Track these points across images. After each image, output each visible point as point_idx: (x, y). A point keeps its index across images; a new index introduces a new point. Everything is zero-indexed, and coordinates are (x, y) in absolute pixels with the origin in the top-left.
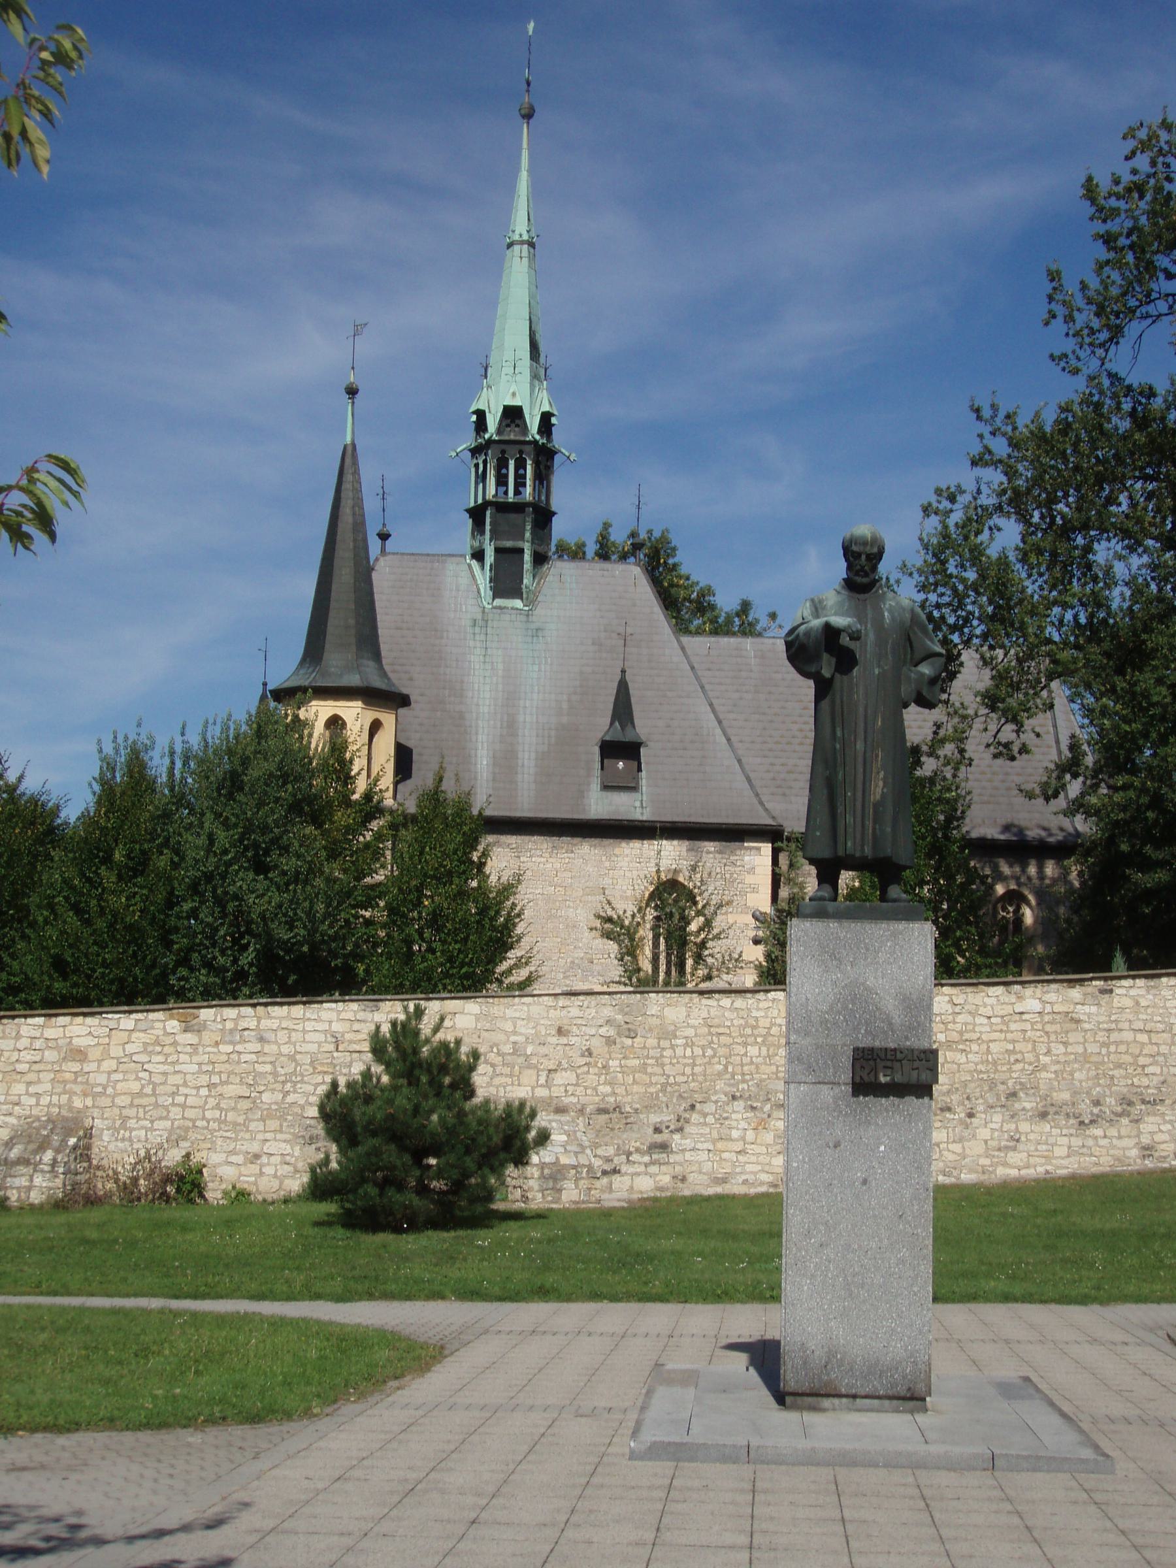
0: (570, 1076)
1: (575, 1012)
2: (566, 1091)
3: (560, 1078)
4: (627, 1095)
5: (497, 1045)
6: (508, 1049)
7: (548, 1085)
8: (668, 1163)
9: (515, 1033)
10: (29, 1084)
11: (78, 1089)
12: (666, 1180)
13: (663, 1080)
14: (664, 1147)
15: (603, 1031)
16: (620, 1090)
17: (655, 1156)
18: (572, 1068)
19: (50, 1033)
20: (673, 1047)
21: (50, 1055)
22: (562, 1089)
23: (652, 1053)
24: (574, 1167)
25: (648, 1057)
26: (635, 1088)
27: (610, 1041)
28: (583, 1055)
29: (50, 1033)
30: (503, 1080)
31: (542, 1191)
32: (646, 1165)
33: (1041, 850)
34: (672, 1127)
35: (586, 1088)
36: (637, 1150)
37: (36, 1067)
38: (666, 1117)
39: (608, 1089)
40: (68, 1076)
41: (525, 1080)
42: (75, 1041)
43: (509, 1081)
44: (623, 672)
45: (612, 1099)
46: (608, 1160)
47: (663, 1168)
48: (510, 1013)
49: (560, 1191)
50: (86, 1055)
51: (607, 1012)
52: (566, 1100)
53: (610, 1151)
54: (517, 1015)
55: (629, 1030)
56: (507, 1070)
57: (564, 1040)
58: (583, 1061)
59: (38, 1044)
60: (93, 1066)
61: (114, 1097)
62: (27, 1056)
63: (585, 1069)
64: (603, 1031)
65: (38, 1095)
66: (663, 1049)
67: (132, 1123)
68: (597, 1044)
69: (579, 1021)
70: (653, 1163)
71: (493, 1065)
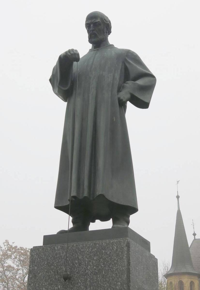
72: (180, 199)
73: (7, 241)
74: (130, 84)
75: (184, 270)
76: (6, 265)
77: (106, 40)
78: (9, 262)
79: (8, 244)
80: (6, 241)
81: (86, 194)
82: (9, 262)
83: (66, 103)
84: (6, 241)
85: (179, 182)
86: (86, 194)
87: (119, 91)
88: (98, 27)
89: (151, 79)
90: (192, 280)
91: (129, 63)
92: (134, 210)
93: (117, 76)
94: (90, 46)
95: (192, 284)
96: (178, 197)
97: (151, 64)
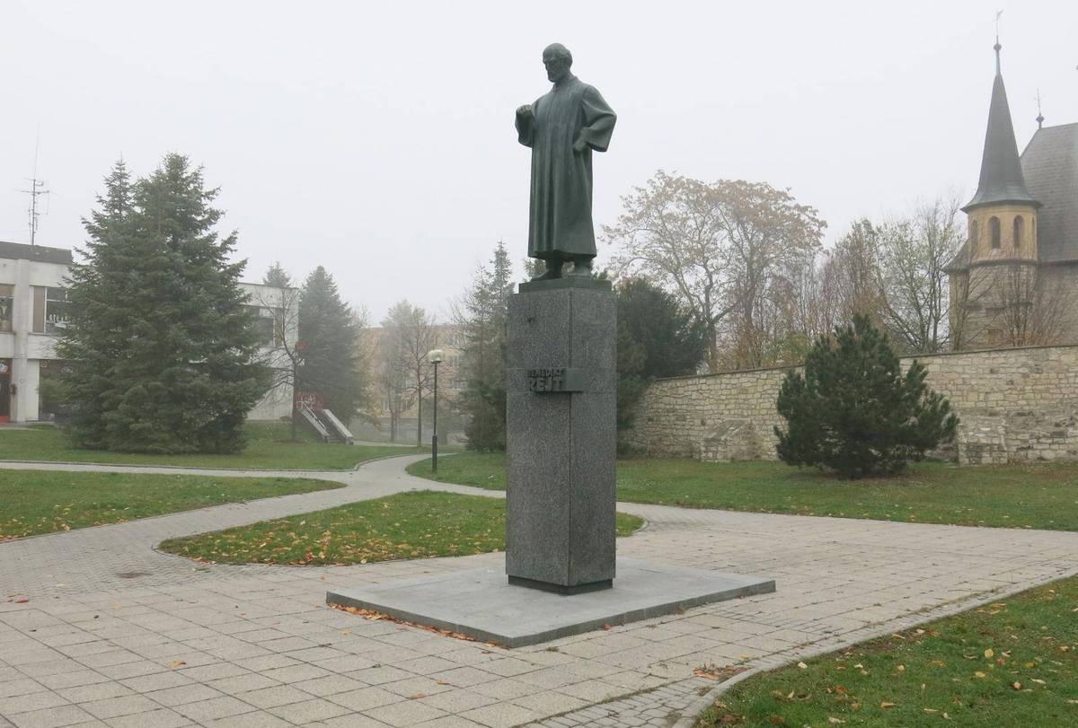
0: (1000, 396)
1: (1002, 360)
2: (997, 404)
3: (992, 397)
4: (1037, 405)
5: (953, 380)
6: (960, 381)
7: (986, 400)
8: (1065, 443)
9: (964, 373)
10: (726, 405)
11: (745, 406)
12: (1063, 453)
13: (1061, 396)
14: (1061, 434)
15: (1021, 370)
16: (1033, 403)
17: (1055, 440)
18: (1002, 391)
19: (733, 381)
20: (1067, 378)
21: (734, 392)
22: (995, 403)
23: (1053, 381)
24: (988, 445)
25: (1050, 384)
26: (1042, 402)
27: (1025, 376)
28: (1007, 384)
29: (733, 381)
30: (957, 398)
31: (968, 457)
32: (1050, 444)
33: (704, 377)
34: (1067, 423)
35: (1010, 402)
36: (1044, 436)
37: (729, 397)
38: (1060, 418)
39: (1024, 402)
40: (741, 401)
41: (970, 397)
42: (744, 385)
43: (961, 398)
44: (579, 392)
45: (1027, 408)
46: (1025, 441)
47: (1061, 447)
48: (960, 362)
49: (981, 457)
50: (747, 390)
51: (1023, 359)
52: (998, 409)
53: (1027, 436)
54: (965, 363)
55: (1038, 369)
56: (959, 393)
57: (995, 376)
58: (1007, 387)
59: (729, 387)
60: (750, 396)
61: (759, 410)
62: (725, 392)
63: (1009, 391)
64: (1021, 370)
65: (729, 410)
66: (1061, 379)
67: (768, 422)
68: (1016, 378)
69: (1004, 365)
70: (1053, 443)
71: (951, 391)
72: (1000, 52)
73: (660, 172)
74: (584, 131)
75: (1002, 197)
76: (665, 212)
77: (568, 72)
78: (671, 208)
79: (664, 177)
80: (659, 171)
81: (545, 249)
82: (671, 208)
83: (530, 149)
84: (659, 171)
85: (1002, 15)
86: (545, 249)
87: (575, 139)
88: (557, 63)
89: (609, 119)
90: (1018, 214)
91: (585, 104)
92: (595, 256)
93: (573, 124)
94: (551, 85)
95: (1018, 222)
96: (997, 48)
97: (612, 99)
